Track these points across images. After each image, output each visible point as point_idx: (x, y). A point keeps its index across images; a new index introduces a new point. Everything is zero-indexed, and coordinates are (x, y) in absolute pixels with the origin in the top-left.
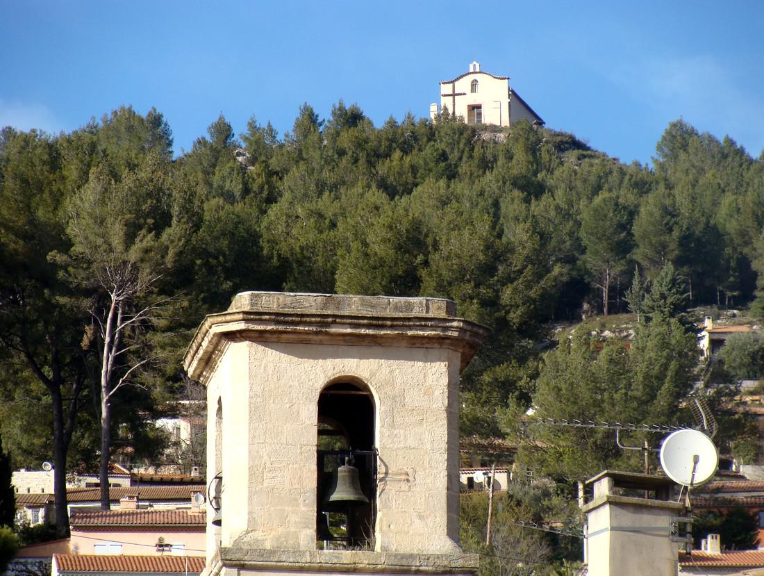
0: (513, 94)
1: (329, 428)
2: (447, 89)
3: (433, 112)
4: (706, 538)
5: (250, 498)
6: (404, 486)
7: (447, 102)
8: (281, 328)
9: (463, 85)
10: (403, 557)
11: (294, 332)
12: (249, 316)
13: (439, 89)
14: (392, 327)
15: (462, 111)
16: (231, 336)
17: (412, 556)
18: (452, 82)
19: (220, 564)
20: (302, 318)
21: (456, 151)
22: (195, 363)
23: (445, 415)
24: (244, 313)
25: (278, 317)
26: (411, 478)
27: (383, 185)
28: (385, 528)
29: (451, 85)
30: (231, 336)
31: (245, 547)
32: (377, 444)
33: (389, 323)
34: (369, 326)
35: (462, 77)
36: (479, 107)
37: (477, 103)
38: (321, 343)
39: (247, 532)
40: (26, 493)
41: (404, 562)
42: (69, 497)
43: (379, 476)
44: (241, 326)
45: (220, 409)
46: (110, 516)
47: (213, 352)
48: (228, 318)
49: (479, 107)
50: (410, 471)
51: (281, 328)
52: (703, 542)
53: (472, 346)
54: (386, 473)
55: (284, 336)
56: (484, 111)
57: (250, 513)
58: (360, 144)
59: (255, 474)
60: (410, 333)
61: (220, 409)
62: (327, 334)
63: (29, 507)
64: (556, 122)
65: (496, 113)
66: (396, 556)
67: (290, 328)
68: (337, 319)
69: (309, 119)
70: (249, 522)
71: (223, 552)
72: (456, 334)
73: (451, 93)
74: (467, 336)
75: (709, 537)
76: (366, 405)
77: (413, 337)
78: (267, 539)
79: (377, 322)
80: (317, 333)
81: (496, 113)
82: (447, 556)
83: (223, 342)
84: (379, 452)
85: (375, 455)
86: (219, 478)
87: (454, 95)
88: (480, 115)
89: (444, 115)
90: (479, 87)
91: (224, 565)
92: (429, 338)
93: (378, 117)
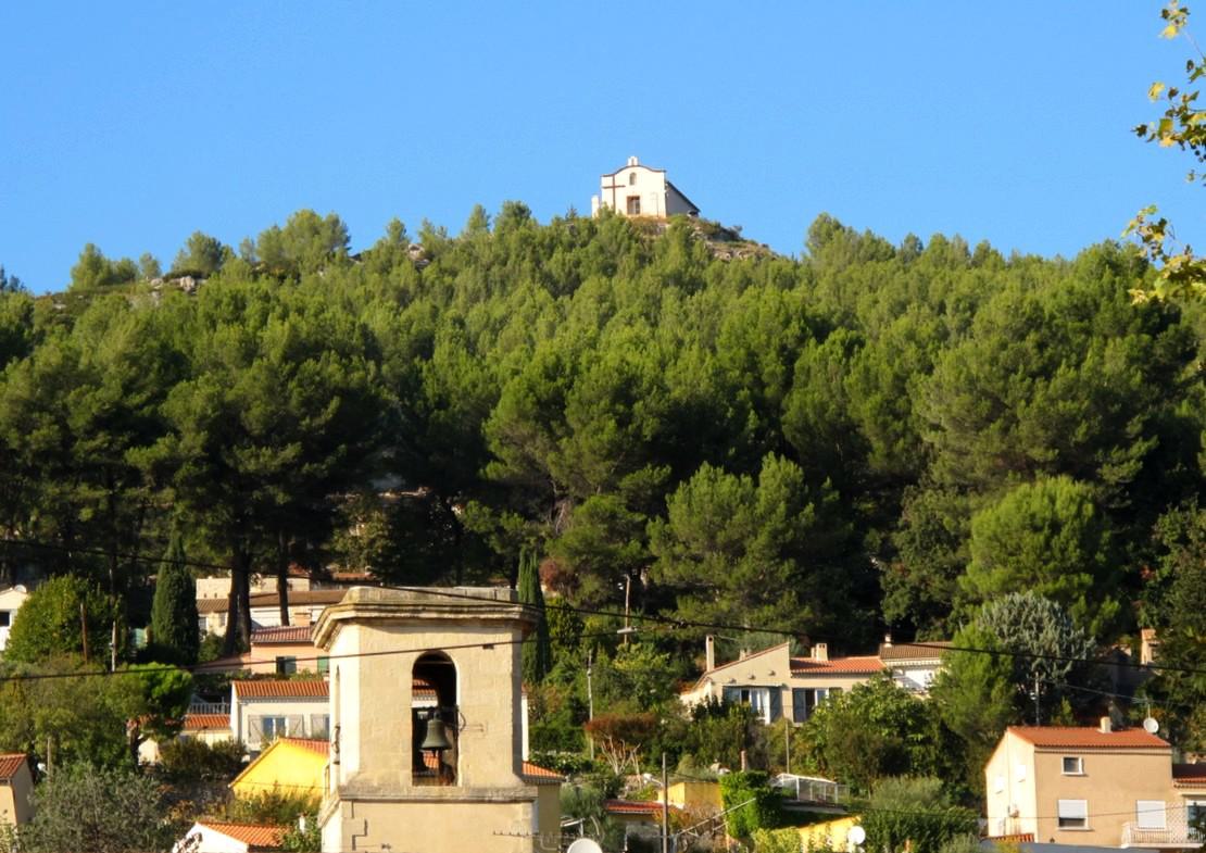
0: (669, 186)
1: (423, 684)
2: (607, 181)
3: (594, 212)
4: (814, 646)
5: (361, 747)
6: (480, 734)
7: (607, 196)
8: (383, 615)
9: (623, 178)
10: (480, 790)
11: (393, 618)
12: (359, 606)
13: (600, 182)
14: (468, 612)
15: (622, 207)
16: (345, 621)
17: (486, 790)
18: (613, 175)
19: (338, 798)
20: (399, 607)
21: (614, 243)
22: (319, 638)
23: (510, 679)
24: (356, 604)
25: (381, 607)
26: (485, 729)
27: (547, 280)
28: (465, 768)
29: (611, 178)
30: (345, 621)
31: (358, 785)
32: (458, 702)
33: (466, 609)
34: (451, 612)
35: (621, 170)
36: (638, 198)
37: (635, 194)
38: (414, 625)
39: (359, 773)
40: (213, 598)
41: (480, 795)
42: (252, 601)
43: (460, 727)
44: (352, 614)
45: (338, 674)
46: (290, 630)
47: (332, 631)
48: (342, 608)
49: (638, 198)
50: (484, 723)
51: (383, 615)
52: (813, 650)
53: (531, 624)
54: (464, 725)
55: (386, 621)
56: (643, 202)
57: (361, 759)
58: (525, 241)
59: (364, 727)
60: (482, 616)
61: (338, 674)
62: (418, 618)
63: (216, 612)
64: (711, 213)
65: (654, 205)
66: (474, 790)
67: (390, 615)
68: (426, 607)
69: (480, 221)
70: (361, 765)
71: (341, 789)
72: (517, 617)
73: (611, 185)
74: (526, 618)
75: (818, 646)
76: (450, 672)
77: (484, 620)
78: (375, 777)
79: (456, 609)
80: (410, 618)
81: (654, 205)
82: (515, 788)
83: (339, 625)
84: (460, 708)
85: (457, 710)
86: (338, 728)
87: (614, 187)
88: (638, 205)
89: (608, 214)
90: (638, 180)
91: (342, 800)
92: (497, 620)
93: (543, 217)
